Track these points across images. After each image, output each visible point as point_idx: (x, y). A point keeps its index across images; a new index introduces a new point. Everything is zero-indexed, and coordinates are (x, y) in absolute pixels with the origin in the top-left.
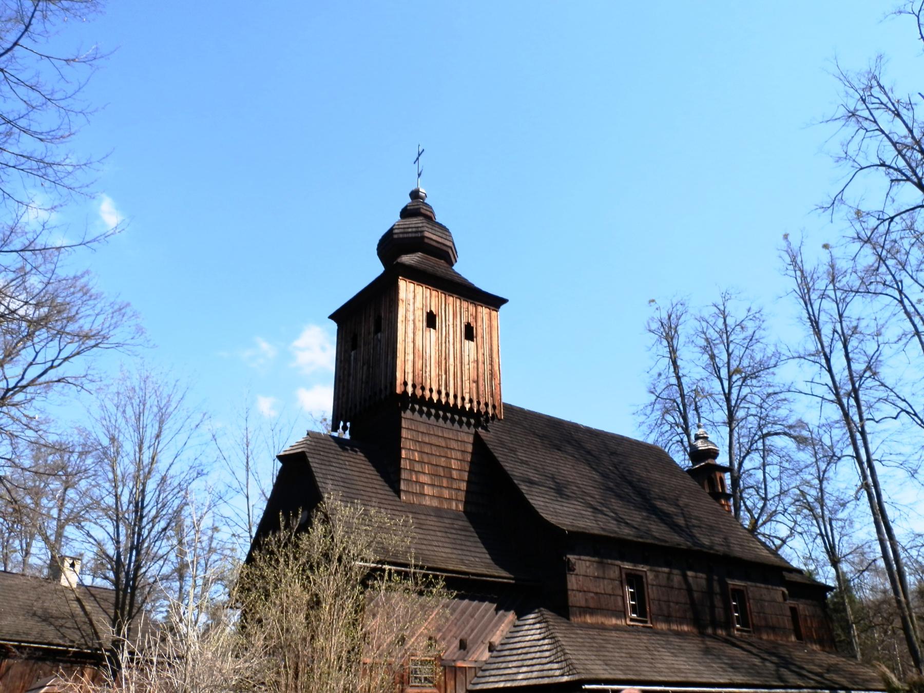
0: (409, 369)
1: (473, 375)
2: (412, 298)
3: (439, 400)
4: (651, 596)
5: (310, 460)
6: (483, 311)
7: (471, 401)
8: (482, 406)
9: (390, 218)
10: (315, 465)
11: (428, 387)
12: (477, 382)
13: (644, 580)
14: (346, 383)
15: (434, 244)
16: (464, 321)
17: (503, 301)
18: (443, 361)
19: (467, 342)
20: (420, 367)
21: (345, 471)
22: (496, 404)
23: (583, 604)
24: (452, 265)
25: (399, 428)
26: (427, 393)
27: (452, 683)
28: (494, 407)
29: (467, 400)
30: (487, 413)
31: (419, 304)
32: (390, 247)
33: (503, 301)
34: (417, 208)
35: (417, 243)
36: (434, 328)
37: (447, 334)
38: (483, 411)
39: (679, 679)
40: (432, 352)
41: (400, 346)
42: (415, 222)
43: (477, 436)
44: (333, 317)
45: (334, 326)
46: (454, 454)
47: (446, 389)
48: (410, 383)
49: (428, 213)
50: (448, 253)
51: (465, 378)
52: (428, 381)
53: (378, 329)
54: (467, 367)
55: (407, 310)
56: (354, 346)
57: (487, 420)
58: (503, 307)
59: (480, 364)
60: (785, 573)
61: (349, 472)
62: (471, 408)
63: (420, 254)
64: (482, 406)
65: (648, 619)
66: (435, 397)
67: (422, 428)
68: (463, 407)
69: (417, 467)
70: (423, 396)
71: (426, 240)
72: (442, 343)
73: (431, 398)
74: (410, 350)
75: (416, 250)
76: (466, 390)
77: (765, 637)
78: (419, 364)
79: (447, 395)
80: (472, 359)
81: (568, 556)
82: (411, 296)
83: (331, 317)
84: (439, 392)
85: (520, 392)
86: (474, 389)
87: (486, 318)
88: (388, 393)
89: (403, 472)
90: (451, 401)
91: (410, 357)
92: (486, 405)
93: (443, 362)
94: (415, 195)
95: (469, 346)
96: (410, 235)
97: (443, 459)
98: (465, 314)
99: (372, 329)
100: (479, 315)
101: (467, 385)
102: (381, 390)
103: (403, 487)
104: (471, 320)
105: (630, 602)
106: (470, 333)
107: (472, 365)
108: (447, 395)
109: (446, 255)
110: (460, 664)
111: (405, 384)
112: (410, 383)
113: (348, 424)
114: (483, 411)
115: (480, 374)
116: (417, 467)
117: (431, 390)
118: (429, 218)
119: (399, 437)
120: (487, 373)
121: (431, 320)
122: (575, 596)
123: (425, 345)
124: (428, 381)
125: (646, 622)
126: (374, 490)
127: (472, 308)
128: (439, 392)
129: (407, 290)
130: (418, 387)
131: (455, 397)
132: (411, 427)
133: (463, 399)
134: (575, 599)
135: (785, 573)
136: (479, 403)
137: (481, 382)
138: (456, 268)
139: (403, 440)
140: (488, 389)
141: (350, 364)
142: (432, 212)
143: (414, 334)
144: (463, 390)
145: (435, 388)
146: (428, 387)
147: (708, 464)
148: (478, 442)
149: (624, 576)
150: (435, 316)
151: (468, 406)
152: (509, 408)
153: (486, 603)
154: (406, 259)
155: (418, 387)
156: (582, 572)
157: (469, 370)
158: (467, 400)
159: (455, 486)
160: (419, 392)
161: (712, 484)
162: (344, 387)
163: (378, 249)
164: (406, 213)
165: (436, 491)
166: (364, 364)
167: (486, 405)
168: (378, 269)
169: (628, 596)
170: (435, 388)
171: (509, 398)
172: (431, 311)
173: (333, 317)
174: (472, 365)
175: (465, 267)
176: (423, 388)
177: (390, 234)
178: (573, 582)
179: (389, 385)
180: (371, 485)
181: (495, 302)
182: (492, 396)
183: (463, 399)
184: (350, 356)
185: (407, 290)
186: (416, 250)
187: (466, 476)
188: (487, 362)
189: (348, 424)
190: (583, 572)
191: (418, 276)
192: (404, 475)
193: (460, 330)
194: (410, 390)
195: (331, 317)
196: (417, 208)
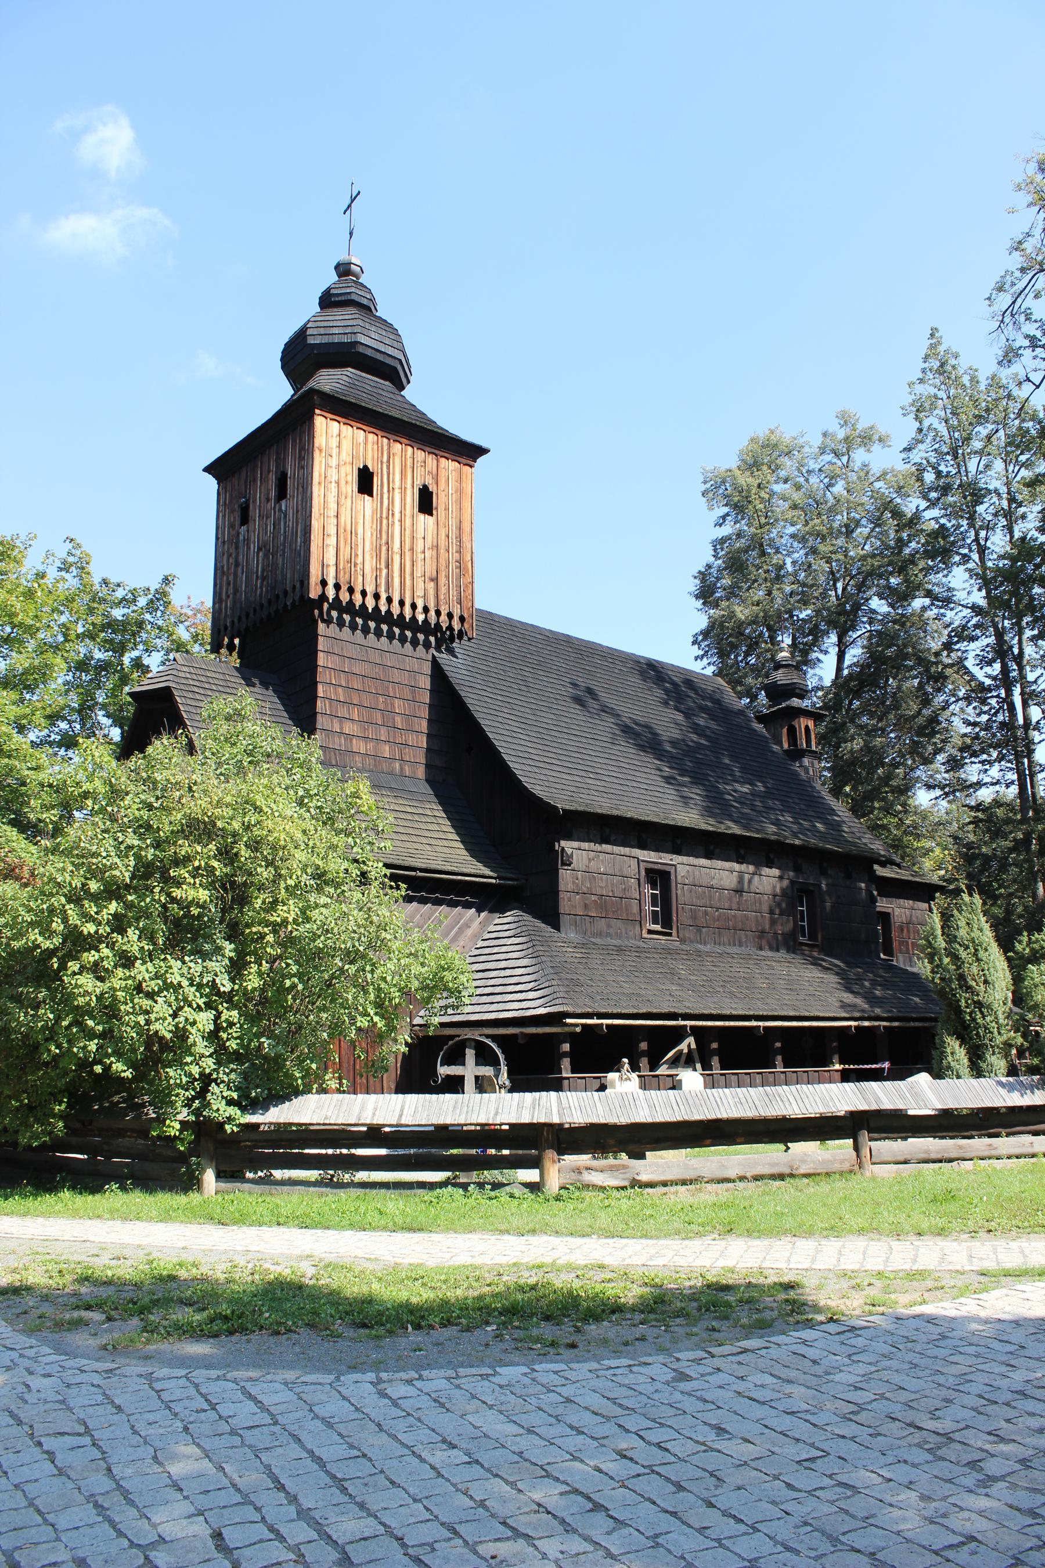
0: (330, 558)
1: (431, 570)
2: (337, 446)
3: (376, 608)
4: (681, 900)
6: (450, 466)
7: (426, 610)
8: (444, 618)
9: (301, 310)
11: (358, 589)
12: (435, 580)
13: (673, 877)
14: (231, 578)
15: (369, 352)
16: (419, 483)
17: (481, 451)
18: (383, 546)
19: (422, 516)
20: (347, 556)
22: (466, 615)
24: (403, 388)
25: (315, 652)
28: (462, 619)
29: (420, 609)
30: (450, 628)
31: (345, 456)
32: (301, 357)
33: (481, 451)
34: (345, 295)
35: (344, 355)
36: (371, 494)
37: (391, 501)
41: (316, 525)
42: (342, 320)
43: (435, 663)
45: (211, 484)
48: (331, 582)
49: (365, 302)
50: (395, 369)
51: (418, 573)
52: (360, 578)
53: (282, 494)
55: (328, 466)
56: (245, 519)
57: (452, 639)
59: (442, 551)
60: (876, 867)
62: (426, 621)
63: (350, 371)
64: (444, 618)
65: (674, 932)
66: (370, 604)
67: (352, 651)
68: (414, 618)
69: (342, 712)
71: (361, 349)
72: (383, 519)
74: (332, 530)
75: (344, 365)
76: (420, 592)
78: (345, 553)
79: (389, 600)
80: (429, 544)
81: (563, 843)
82: (334, 442)
83: (208, 469)
84: (377, 597)
85: (505, 592)
87: (453, 477)
88: (297, 598)
91: (332, 541)
92: (450, 616)
93: (384, 548)
94: (344, 270)
97: (381, 699)
98: (419, 471)
99: (273, 494)
100: (443, 474)
102: (286, 593)
105: (648, 908)
106: (426, 502)
107: (428, 554)
108: (389, 600)
109: (393, 373)
111: (324, 583)
112: (331, 582)
113: (237, 641)
114: (444, 626)
115: (443, 568)
116: (342, 712)
117: (364, 593)
118: (367, 309)
119: (314, 667)
120: (453, 565)
121: (365, 482)
122: (569, 900)
123: (355, 523)
127: (431, 460)
128: (377, 597)
129: (327, 430)
130: (344, 588)
131: (402, 603)
132: (335, 648)
133: (414, 606)
134: (568, 903)
135: (876, 867)
136: (438, 613)
137: (442, 580)
138: (409, 393)
139: (320, 669)
140: (453, 593)
142: (372, 300)
144: (415, 592)
145: (370, 590)
147: (788, 707)
148: (441, 681)
149: (643, 873)
150: (372, 474)
151: (421, 617)
152: (488, 619)
153: (429, 905)
155: (344, 588)
156: (582, 867)
157: (425, 566)
158: (420, 609)
162: (229, 584)
163: (283, 367)
164: (328, 301)
166: (259, 549)
167: (450, 616)
168: (282, 392)
169: (648, 900)
170: (370, 590)
171: (484, 601)
172: (366, 467)
175: (426, 395)
176: (351, 590)
177: (300, 337)
178: (565, 877)
179: (298, 585)
181: (469, 452)
183: (414, 606)
184: (238, 534)
185: (327, 430)
186: (344, 365)
188: (453, 548)
189: (237, 641)
190: (587, 865)
191: (346, 409)
193: (412, 499)
194: (331, 593)
195: (208, 469)
196: (345, 295)
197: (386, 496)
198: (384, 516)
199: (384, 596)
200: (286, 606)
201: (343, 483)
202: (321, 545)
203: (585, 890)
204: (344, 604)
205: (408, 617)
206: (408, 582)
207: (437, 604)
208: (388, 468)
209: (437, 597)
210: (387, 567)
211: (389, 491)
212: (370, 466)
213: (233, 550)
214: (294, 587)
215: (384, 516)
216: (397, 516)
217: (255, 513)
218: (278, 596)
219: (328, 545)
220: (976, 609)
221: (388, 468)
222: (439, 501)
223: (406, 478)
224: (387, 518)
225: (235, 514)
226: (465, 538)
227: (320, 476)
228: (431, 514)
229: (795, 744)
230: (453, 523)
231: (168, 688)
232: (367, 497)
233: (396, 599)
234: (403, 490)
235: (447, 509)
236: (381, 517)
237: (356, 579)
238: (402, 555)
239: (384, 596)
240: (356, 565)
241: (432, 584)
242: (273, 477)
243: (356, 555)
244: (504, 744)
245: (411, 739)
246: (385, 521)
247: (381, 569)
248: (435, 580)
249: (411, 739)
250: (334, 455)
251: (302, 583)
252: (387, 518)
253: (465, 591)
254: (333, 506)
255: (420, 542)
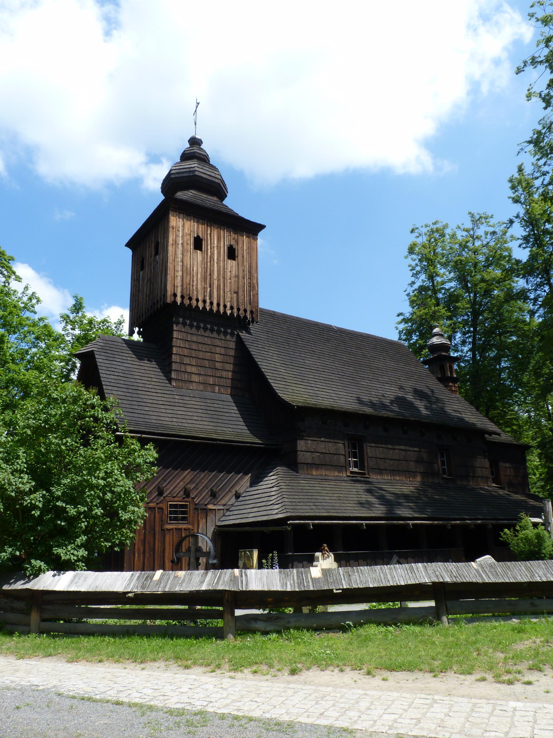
0: (178, 282)
1: (234, 288)
5: (96, 356)
7: (232, 308)
8: (241, 312)
10: (100, 361)
11: (194, 298)
12: (237, 293)
14: (137, 297)
18: (207, 276)
20: (188, 281)
21: (126, 365)
22: (254, 310)
23: (310, 461)
26: (194, 303)
27: (204, 520)
29: (228, 307)
36: (201, 250)
38: (242, 316)
39: (373, 515)
40: (198, 270)
42: (193, 164)
44: (128, 245)
45: (129, 252)
46: (218, 350)
47: (210, 298)
48: (179, 295)
51: (227, 290)
52: (195, 292)
53: (157, 253)
54: (229, 281)
56: (142, 268)
58: (261, 234)
61: (130, 366)
64: (241, 312)
68: (225, 312)
69: (187, 361)
70: (190, 305)
73: (197, 306)
74: (180, 268)
77: (314, 473)
79: (211, 303)
84: (204, 302)
86: (235, 299)
88: (162, 303)
89: (174, 364)
90: (215, 308)
91: (180, 274)
92: (245, 311)
93: (208, 277)
95: (231, 264)
96: (185, 175)
101: (229, 295)
103: (173, 375)
104: (233, 243)
106: (232, 254)
108: (211, 303)
109: (218, 190)
110: (210, 507)
111: (175, 295)
112: (179, 295)
114: (242, 316)
115: (240, 286)
117: (197, 300)
121: (198, 244)
122: (304, 455)
124: (195, 292)
125: (364, 474)
126: (150, 379)
128: (204, 302)
130: (186, 298)
131: (218, 305)
133: (225, 306)
134: (303, 457)
135: (486, 436)
136: (238, 309)
137: (241, 293)
141: (139, 282)
143: (183, 254)
144: (225, 300)
145: (200, 298)
146: (195, 298)
150: (202, 240)
151: (229, 312)
152: (273, 315)
154: (180, 195)
158: (228, 307)
159: (218, 375)
160: (187, 302)
161: (442, 369)
162: (136, 300)
164: (186, 157)
165: (201, 379)
166: (148, 282)
167: (245, 311)
170: (200, 298)
172: (198, 236)
173: (128, 245)
174: (233, 280)
175: (234, 203)
176: (190, 299)
180: (147, 375)
181: (253, 229)
182: (250, 304)
183: (225, 306)
187: (230, 367)
192: (174, 366)
193: (224, 251)
194: (179, 300)
197: (209, 251)
198: (209, 261)
199: (208, 301)
200: (158, 308)
201: (185, 244)
202: (173, 276)
203: (313, 450)
204: (194, 306)
205: (222, 311)
206: (222, 294)
207: (238, 305)
208: (211, 236)
209: (238, 301)
210: (210, 287)
211: (211, 248)
212: (200, 236)
213: (137, 284)
214: (161, 298)
215: (209, 261)
216: (216, 260)
217: (146, 264)
218: (154, 303)
219: (177, 276)
220: (506, 242)
221: (211, 236)
222: (239, 253)
223: (220, 241)
224: (210, 262)
225: (139, 264)
226: (253, 271)
227: (173, 241)
228: (235, 260)
229: (445, 374)
230: (246, 264)
231: (93, 351)
232: (199, 252)
233: (228, 305)
234: (219, 247)
235: (243, 257)
236: (207, 261)
237: (193, 293)
238: (219, 280)
239: (208, 301)
240: (193, 286)
241: (235, 295)
242: (153, 245)
243: (193, 281)
244: (269, 374)
245: (224, 374)
246: (209, 264)
247: (207, 288)
248: (237, 293)
249: (224, 374)
250: (181, 230)
251: (164, 295)
252: (210, 262)
253: (254, 299)
254: (180, 256)
255: (229, 274)
